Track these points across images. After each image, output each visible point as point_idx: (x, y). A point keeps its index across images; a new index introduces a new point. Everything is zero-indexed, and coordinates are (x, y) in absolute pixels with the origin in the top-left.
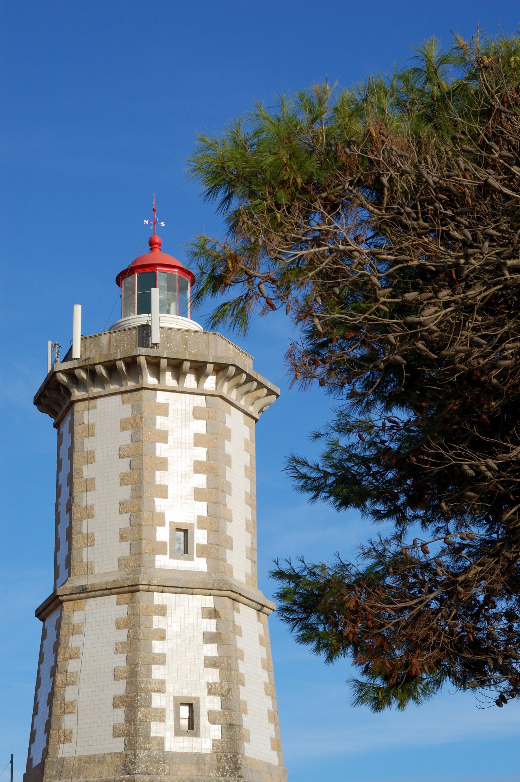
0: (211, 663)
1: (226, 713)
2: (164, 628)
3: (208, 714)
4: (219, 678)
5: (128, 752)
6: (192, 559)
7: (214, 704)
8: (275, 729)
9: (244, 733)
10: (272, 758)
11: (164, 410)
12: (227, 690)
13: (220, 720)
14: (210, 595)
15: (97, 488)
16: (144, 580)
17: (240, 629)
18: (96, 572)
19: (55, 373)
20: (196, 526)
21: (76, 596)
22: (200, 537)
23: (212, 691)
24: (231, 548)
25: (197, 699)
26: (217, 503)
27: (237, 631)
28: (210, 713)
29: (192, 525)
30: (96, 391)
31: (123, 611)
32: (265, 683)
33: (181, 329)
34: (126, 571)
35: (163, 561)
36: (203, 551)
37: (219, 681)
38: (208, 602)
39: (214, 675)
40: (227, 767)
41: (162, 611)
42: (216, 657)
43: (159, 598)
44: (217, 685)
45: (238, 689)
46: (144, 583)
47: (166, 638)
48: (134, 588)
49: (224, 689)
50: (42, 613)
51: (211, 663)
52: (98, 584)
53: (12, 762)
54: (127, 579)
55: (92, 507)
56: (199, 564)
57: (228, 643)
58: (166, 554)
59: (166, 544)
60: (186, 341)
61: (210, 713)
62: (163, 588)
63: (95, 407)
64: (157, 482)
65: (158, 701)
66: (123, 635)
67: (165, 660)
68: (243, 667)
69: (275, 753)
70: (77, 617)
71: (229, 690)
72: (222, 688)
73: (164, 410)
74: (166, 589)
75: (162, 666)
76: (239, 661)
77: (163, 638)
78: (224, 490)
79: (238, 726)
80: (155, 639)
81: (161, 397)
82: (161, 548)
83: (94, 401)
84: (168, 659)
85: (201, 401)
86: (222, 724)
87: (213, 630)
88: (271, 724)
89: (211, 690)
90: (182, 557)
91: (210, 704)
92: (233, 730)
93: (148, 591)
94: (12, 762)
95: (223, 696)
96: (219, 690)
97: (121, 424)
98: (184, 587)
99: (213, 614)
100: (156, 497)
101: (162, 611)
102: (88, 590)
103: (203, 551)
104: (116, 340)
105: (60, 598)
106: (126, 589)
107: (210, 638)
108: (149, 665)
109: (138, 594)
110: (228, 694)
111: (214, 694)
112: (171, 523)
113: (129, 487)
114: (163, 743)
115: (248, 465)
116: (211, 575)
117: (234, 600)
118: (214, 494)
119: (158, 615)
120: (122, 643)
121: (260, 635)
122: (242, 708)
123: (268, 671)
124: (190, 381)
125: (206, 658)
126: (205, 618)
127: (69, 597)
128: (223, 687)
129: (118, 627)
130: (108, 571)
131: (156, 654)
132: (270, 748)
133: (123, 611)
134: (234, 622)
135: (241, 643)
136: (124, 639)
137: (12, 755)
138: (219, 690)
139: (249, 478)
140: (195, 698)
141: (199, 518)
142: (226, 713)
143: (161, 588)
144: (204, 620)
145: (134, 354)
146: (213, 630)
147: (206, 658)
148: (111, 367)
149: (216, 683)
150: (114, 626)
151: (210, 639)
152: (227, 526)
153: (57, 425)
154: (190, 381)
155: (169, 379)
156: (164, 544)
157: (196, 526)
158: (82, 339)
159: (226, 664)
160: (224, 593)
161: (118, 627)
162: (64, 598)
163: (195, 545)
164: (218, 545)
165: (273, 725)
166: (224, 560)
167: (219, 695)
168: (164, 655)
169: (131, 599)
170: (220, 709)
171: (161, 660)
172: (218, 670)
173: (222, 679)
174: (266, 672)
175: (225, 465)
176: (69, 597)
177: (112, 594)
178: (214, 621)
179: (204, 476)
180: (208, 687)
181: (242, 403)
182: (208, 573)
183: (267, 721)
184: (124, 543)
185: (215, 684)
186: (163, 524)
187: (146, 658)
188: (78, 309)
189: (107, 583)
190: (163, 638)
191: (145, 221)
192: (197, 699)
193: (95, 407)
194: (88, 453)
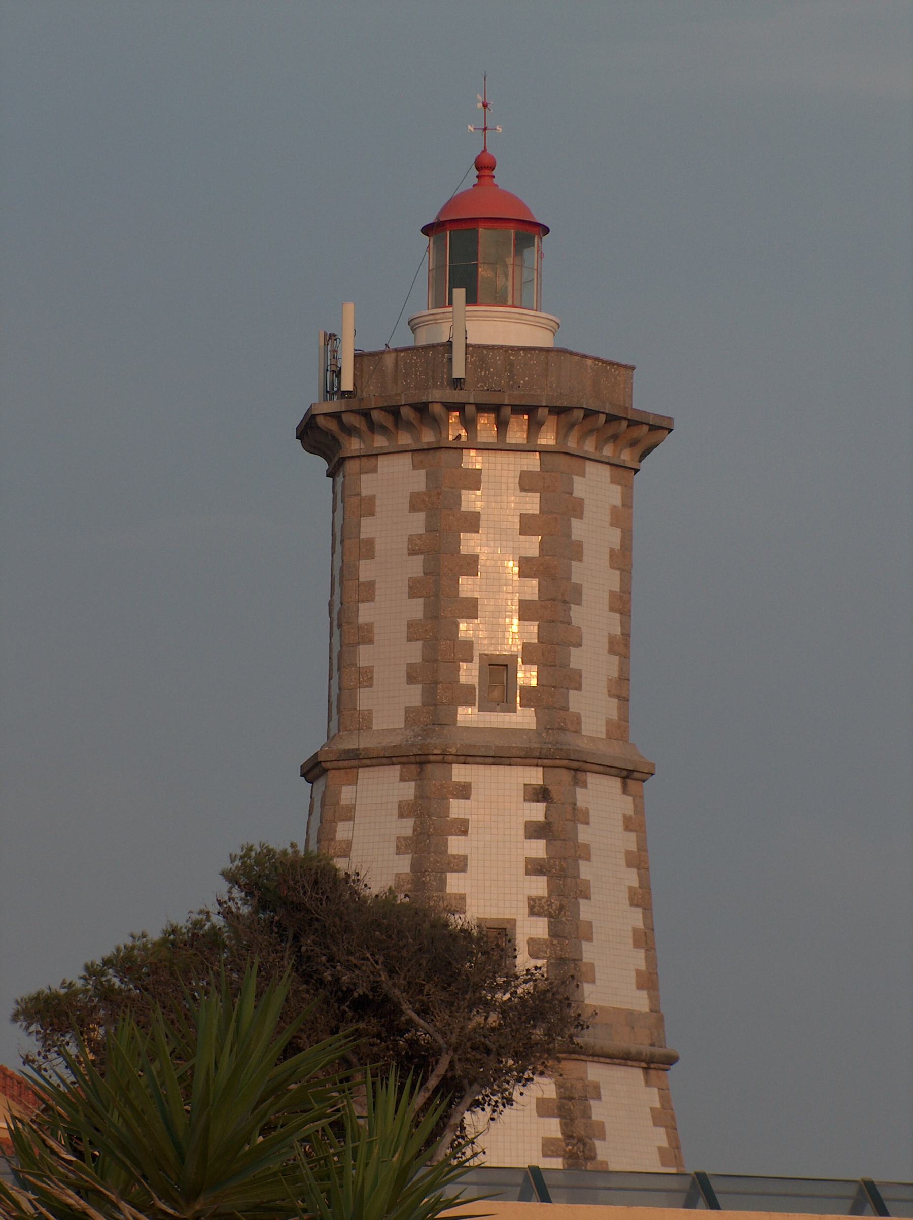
0: (535, 868)
1: (555, 942)
2: (467, 817)
3: (528, 944)
4: (546, 891)
6: (514, 710)
7: (539, 928)
8: (646, 957)
9: (584, 970)
11: (474, 480)
13: (546, 953)
14: (537, 766)
15: (377, 598)
16: (435, 748)
17: (586, 813)
18: (374, 728)
19: (314, 416)
20: (520, 660)
21: (345, 764)
22: (527, 676)
23: (536, 910)
25: (513, 922)
26: (553, 622)
27: (580, 816)
28: (531, 942)
29: (514, 657)
30: (380, 442)
31: (408, 790)
32: (630, 888)
33: (502, 347)
34: (414, 731)
35: (467, 715)
36: (530, 697)
37: (546, 895)
38: (535, 776)
39: (539, 886)
41: (464, 791)
42: (543, 859)
43: (460, 773)
44: (544, 901)
45: (577, 906)
46: (436, 752)
47: (469, 832)
48: (423, 758)
49: (554, 907)
50: (313, 770)
51: (535, 868)
52: (373, 749)
54: (412, 745)
56: (523, 718)
57: (562, 837)
59: (475, 688)
60: (511, 364)
61: (531, 942)
62: (466, 758)
63: (374, 470)
64: (464, 550)
66: (407, 827)
67: (466, 865)
69: (644, 994)
70: (347, 794)
71: (561, 908)
72: (550, 905)
73: (474, 480)
74: (470, 759)
75: (462, 874)
76: (581, 863)
77: (465, 833)
78: (567, 599)
79: (574, 960)
80: (452, 835)
81: (474, 460)
82: (466, 696)
83: (373, 460)
85: (532, 462)
86: (548, 959)
87: (541, 818)
88: (638, 950)
89: (535, 908)
90: (498, 708)
93: (443, 762)
95: (550, 916)
96: (546, 907)
97: (411, 501)
98: (499, 755)
99: (540, 794)
100: (459, 618)
101: (464, 791)
102: (361, 757)
104: (406, 363)
105: (323, 765)
106: (412, 759)
107: (534, 831)
108: (443, 872)
109: (429, 767)
110: (560, 913)
111: (539, 914)
113: (421, 600)
116: (540, 735)
117: (576, 770)
118: (552, 609)
119: (458, 798)
120: (405, 839)
121: (624, 816)
122: (585, 933)
123: (639, 869)
124: (517, 434)
125: (528, 861)
126: (529, 801)
127: (335, 764)
128: (552, 903)
129: (401, 815)
130: (391, 727)
131: (453, 855)
132: (634, 986)
133: (408, 790)
134: (575, 804)
136: (409, 832)
138: (546, 907)
139: (618, 569)
140: (509, 921)
142: (555, 942)
143: (462, 759)
144: (527, 804)
145: (424, 399)
146: (541, 818)
147: (528, 861)
148: (394, 412)
149: (543, 898)
150: (396, 812)
151: (535, 831)
152: (572, 654)
153: (331, 474)
154: (517, 434)
155: (486, 425)
156: (471, 688)
157: (520, 660)
158: (355, 356)
160: (558, 762)
161: (401, 815)
162: (328, 765)
164: (555, 687)
165: (643, 951)
166: (565, 708)
167: (545, 916)
168: (465, 858)
169: (420, 773)
170: (547, 937)
171: (462, 828)
172: (545, 877)
173: (550, 892)
174: (635, 871)
175: (571, 559)
176: (335, 764)
177: (393, 764)
178: (542, 806)
179: (535, 582)
180: (529, 904)
182: (537, 732)
183: (630, 945)
184: (413, 686)
186: (470, 660)
187: (438, 862)
188: (349, 309)
189: (385, 748)
190: (465, 833)
191: (470, 127)
192: (513, 922)
193: (374, 470)
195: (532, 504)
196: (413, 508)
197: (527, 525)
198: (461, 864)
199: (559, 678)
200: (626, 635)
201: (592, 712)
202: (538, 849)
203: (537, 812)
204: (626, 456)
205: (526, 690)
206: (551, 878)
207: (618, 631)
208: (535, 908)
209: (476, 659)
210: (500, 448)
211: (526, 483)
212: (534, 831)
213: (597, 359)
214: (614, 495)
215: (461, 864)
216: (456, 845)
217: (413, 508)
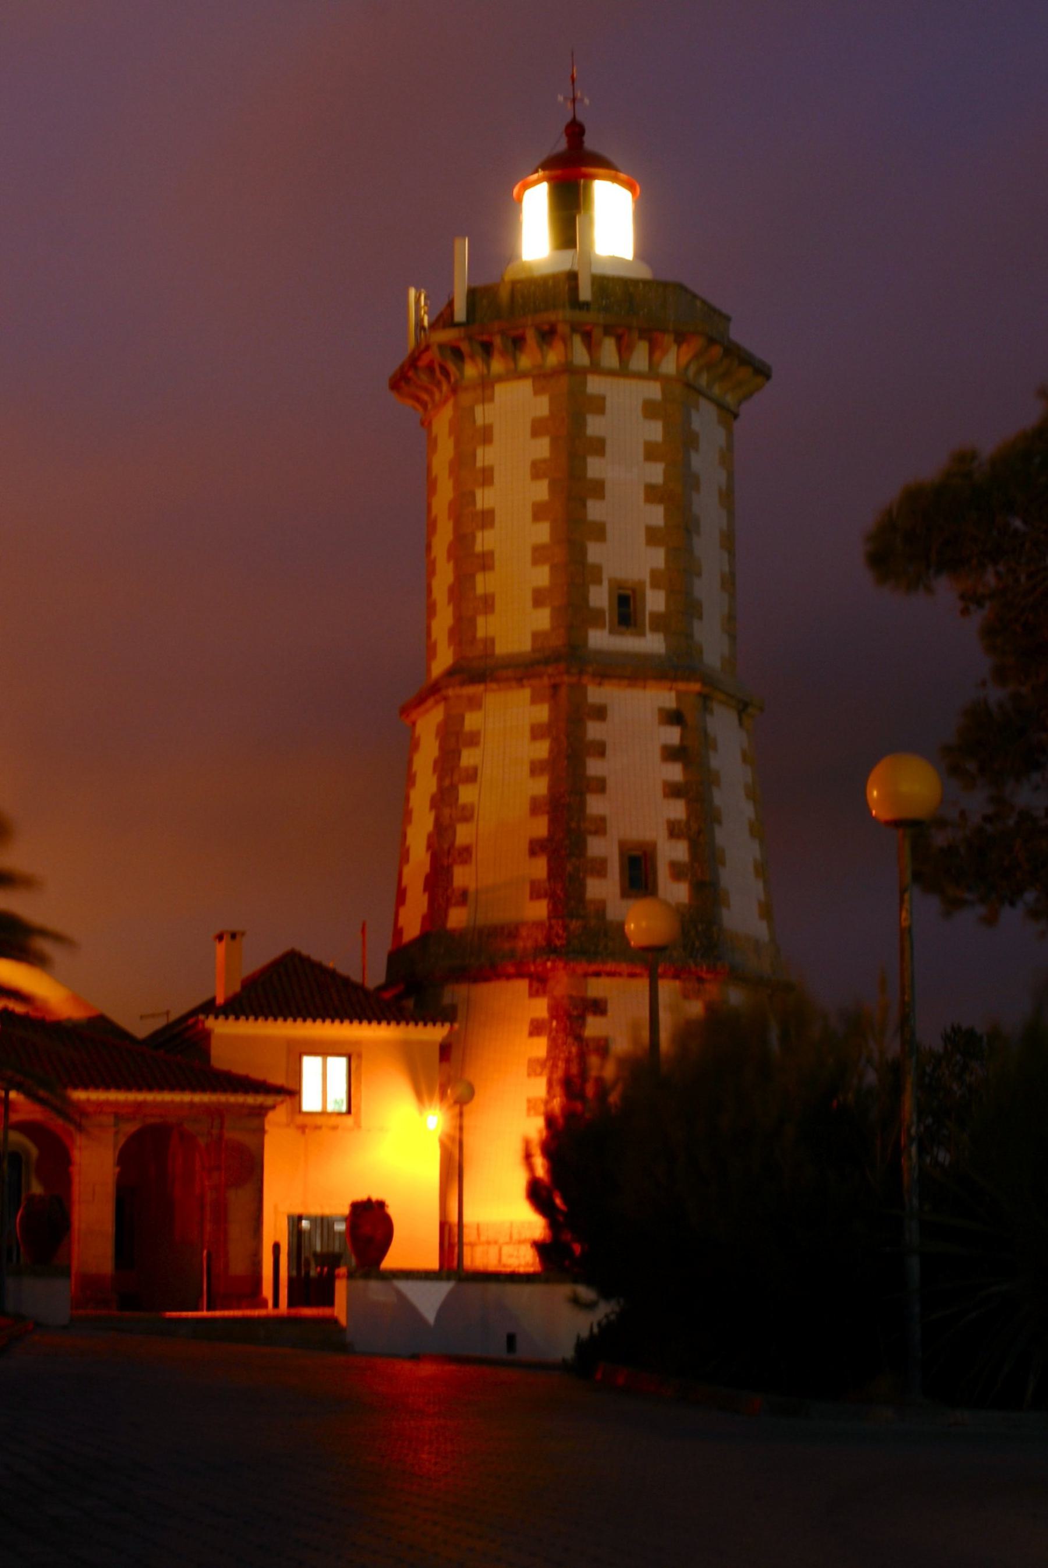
0: (673, 791)
5: (553, 921)
6: (643, 634)
7: (678, 851)
10: (760, 929)
12: (699, 828)
20: (648, 584)
22: (655, 601)
24: (700, 618)
25: (653, 846)
27: (708, 742)
36: (660, 623)
38: (665, 697)
39: (677, 810)
40: (697, 944)
51: (673, 791)
53: (363, 931)
55: (491, 554)
56: (653, 643)
58: (603, 626)
59: (644, 583)
65: (597, 847)
68: (719, 798)
71: (699, 832)
82: (595, 618)
84: (610, 783)
85: (653, 390)
89: (674, 831)
91: (673, 851)
92: (707, 890)
94: (363, 931)
98: (636, 671)
99: (674, 717)
103: (660, 623)
107: (671, 754)
112: (610, 581)
114: (604, 910)
115: (724, 488)
135: (715, 762)
137: (364, 924)
141: (654, 573)
159: (696, 791)
163: (647, 613)
173: (689, 816)
181: (716, 390)
185: (679, 822)
186: (599, 581)
194: (484, 470)
195: (655, 431)
196: (535, 433)
197: (651, 453)
198: (600, 786)
199: (685, 608)
200: (732, 574)
201: (712, 643)
202: (675, 772)
203: (673, 735)
204: (730, 399)
205: (654, 616)
206: (689, 803)
207: (727, 569)
208: (674, 831)
209: (605, 583)
210: (623, 372)
211: (650, 410)
212: (671, 754)
213: (704, 302)
214: (720, 435)
215: (600, 786)
216: (594, 767)
217: (535, 433)
